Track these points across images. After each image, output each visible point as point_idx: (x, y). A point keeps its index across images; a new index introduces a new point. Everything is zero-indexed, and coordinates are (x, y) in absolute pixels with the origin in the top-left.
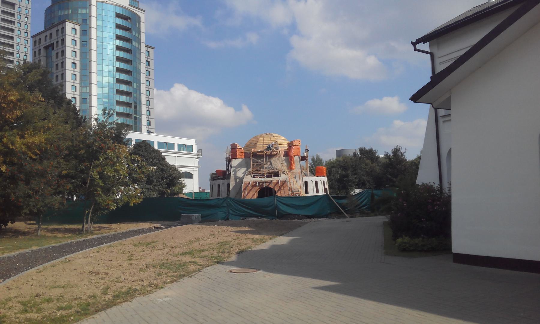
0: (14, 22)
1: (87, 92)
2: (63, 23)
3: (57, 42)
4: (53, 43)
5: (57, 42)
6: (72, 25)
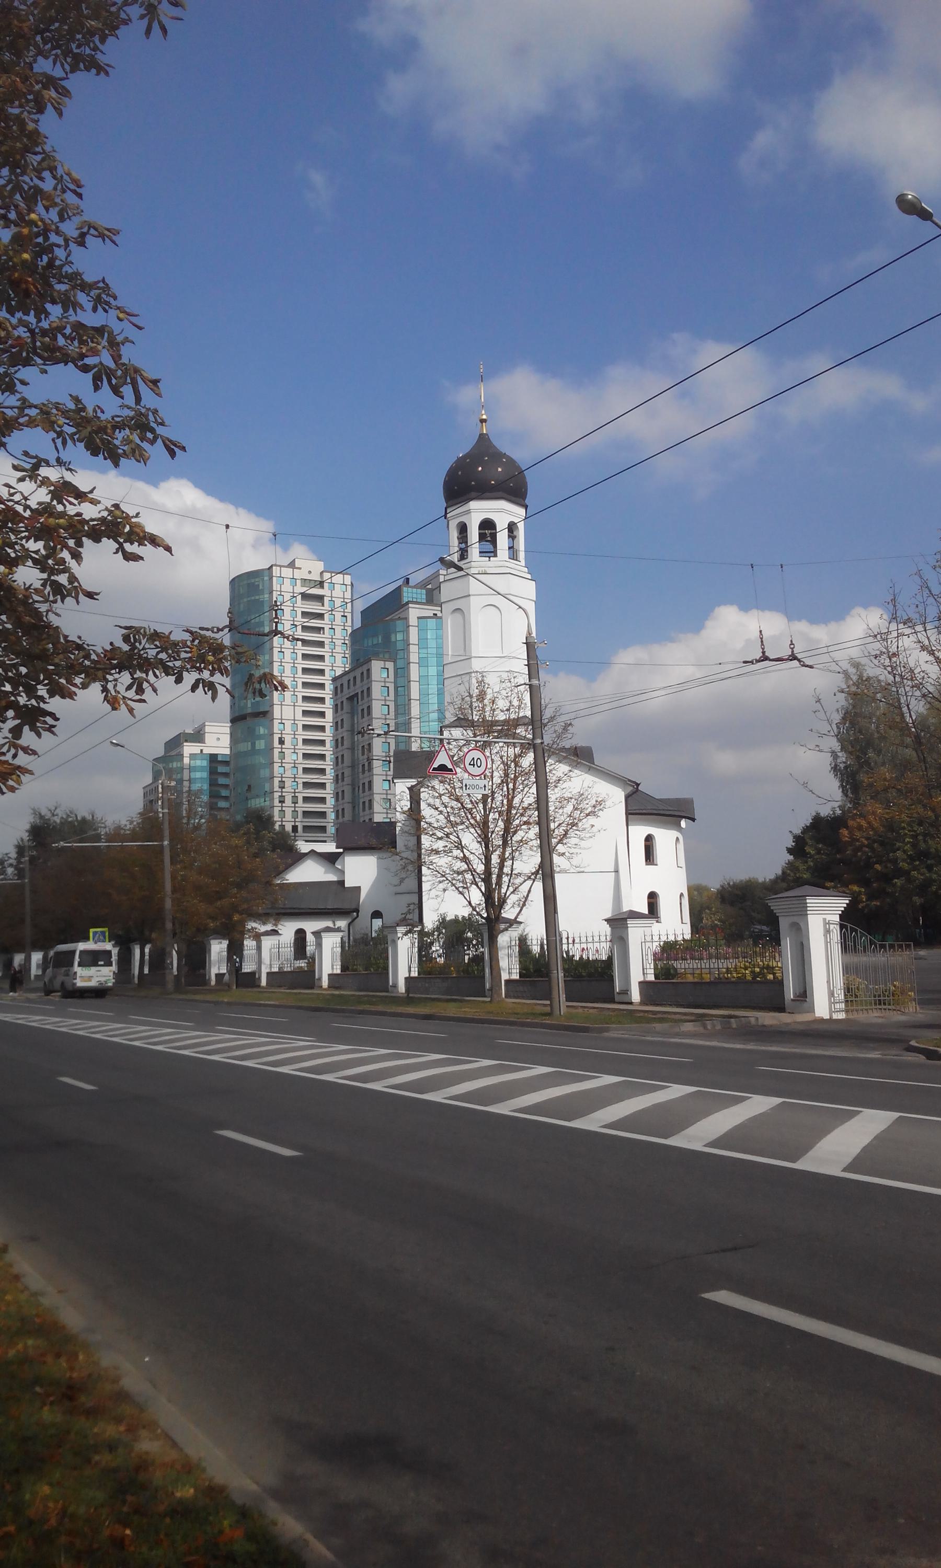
0: (323, 628)
1: (404, 658)
2: (368, 662)
3: (362, 692)
4: (358, 693)
5: (362, 692)
6: (381, 664)
